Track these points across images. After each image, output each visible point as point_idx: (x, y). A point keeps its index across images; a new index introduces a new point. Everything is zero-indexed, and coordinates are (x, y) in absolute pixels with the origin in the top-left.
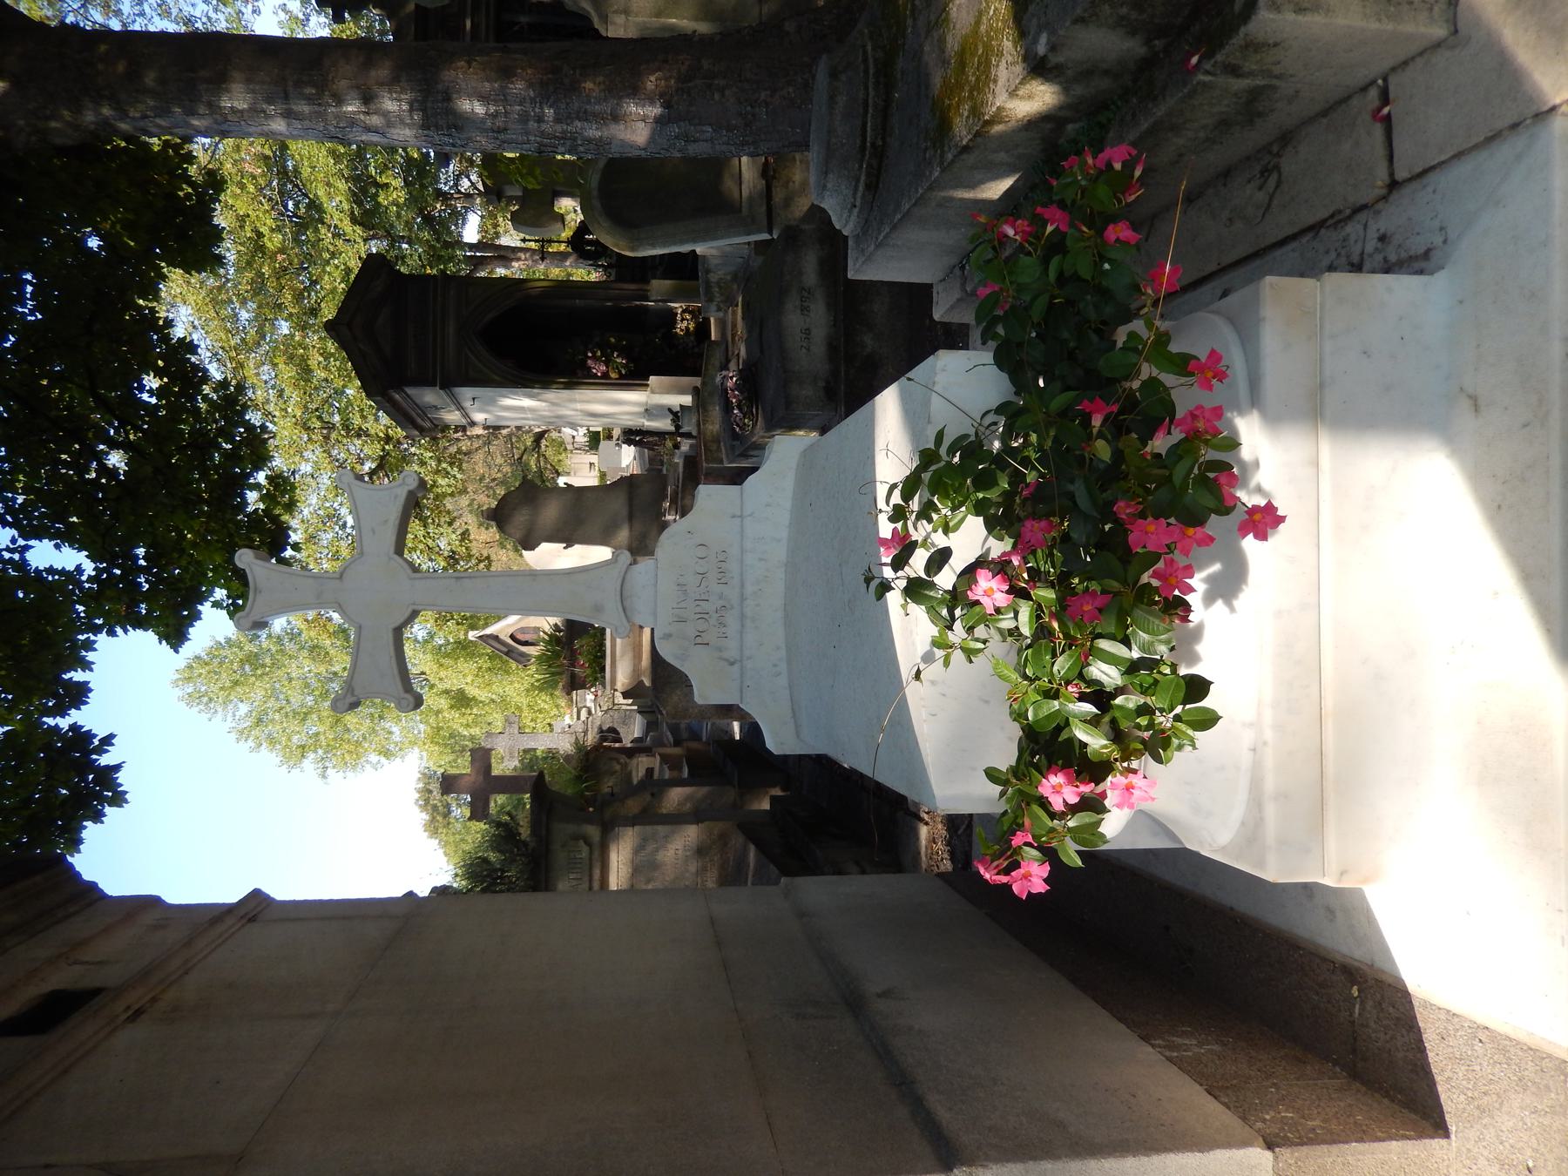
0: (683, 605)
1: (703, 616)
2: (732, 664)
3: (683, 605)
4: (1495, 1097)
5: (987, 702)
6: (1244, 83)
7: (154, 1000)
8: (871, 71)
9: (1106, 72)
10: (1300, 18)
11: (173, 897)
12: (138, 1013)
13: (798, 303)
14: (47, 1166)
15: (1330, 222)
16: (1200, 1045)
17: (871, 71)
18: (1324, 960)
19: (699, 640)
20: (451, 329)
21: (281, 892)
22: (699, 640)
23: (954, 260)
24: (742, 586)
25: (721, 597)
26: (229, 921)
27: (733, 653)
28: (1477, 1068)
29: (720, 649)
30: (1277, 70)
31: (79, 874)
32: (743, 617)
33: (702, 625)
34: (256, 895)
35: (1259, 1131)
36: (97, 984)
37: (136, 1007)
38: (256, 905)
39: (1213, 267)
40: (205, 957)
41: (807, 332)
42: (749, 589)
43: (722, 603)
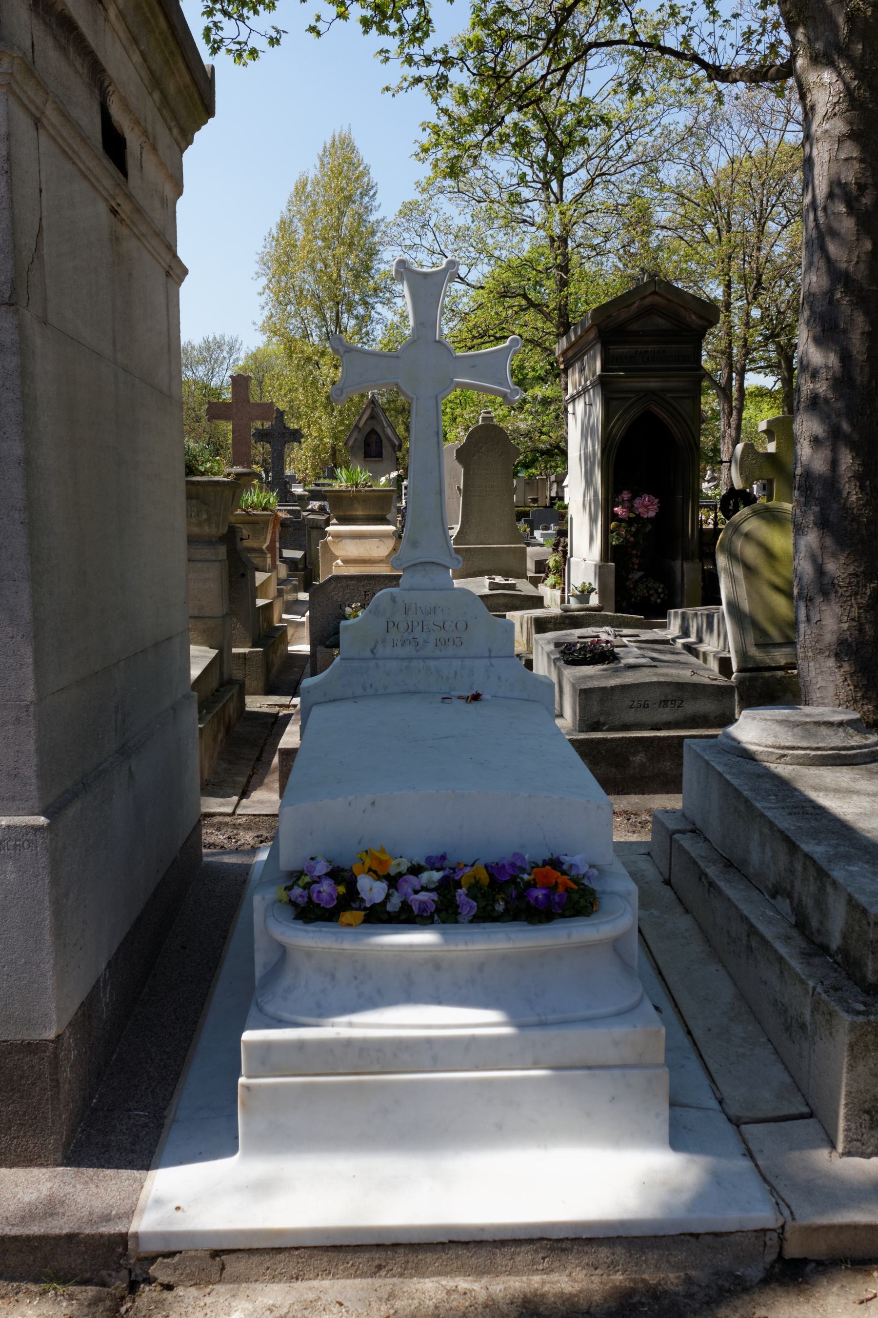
0: (419, 612)
1: (410, 628)
2: (372, 651)
3: (419, 612)
4: (96, 1191)
5: (360, 843)
6: (808, 1017)
7: (122, 221)
8: (842, 752)
9: (821, 923)
10: (846, 1048)
11: (182, 205)
12: (114, 212)
13: (670, 697)
14: (41, 191)
15: (714, 1087)
16: (107, 1005)
17: (842, 752)
18: (172, 1093)
19: (391, 625)
20: (654, 384)
21: (186, 290)
22: (391, 625)
23: (699, 824)
24: (435, 658)
25: (426, 642)
26: (168, 258)
27: (380, 651)
28: (114, 1182)
29: (384, 641)
30: (817, 1038)
31: (199, 129)
32: (410, 659)
33: (403, 626)
34: (185, 272)
35: (64, 1032)
36: (129, 177)
37: (119, 211)
38: (176, 272)
39: (712, 1067)
40: (146, 247)
41: (646, 706)
42: (432, 664)
43: (421, 643)
